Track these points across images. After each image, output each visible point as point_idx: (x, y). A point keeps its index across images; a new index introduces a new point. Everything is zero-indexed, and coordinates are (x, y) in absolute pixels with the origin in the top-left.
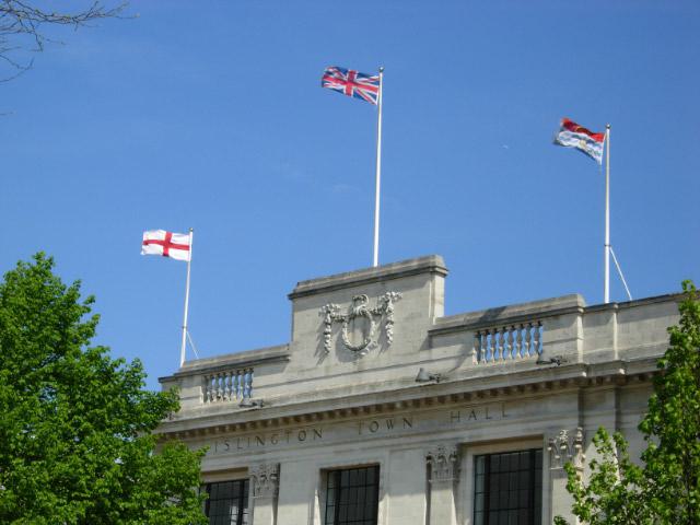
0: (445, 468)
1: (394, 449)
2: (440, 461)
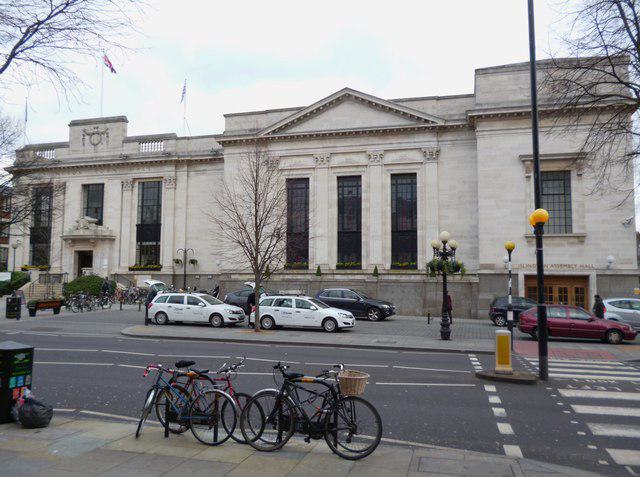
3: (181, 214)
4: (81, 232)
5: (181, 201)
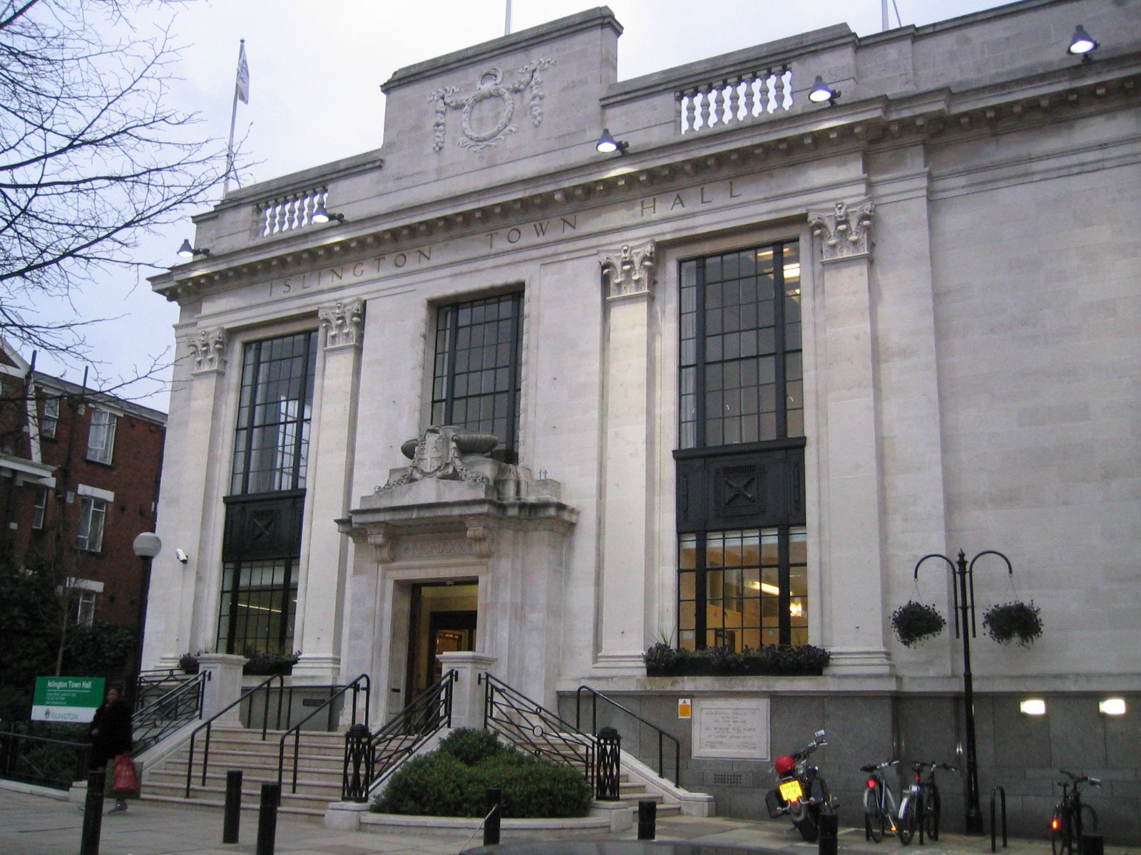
1: (545, 262)
2: (205, 348)
4: (427, 492)
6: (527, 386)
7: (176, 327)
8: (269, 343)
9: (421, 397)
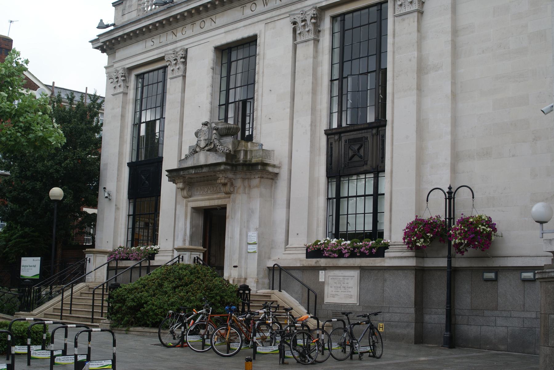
0: (307, 29)
2: (303, 23)
3: (439, 83)
5: (438, 45)
6: (257, 95)
7: (106, 68)
8: (351, 15)
9: (211, 103)
